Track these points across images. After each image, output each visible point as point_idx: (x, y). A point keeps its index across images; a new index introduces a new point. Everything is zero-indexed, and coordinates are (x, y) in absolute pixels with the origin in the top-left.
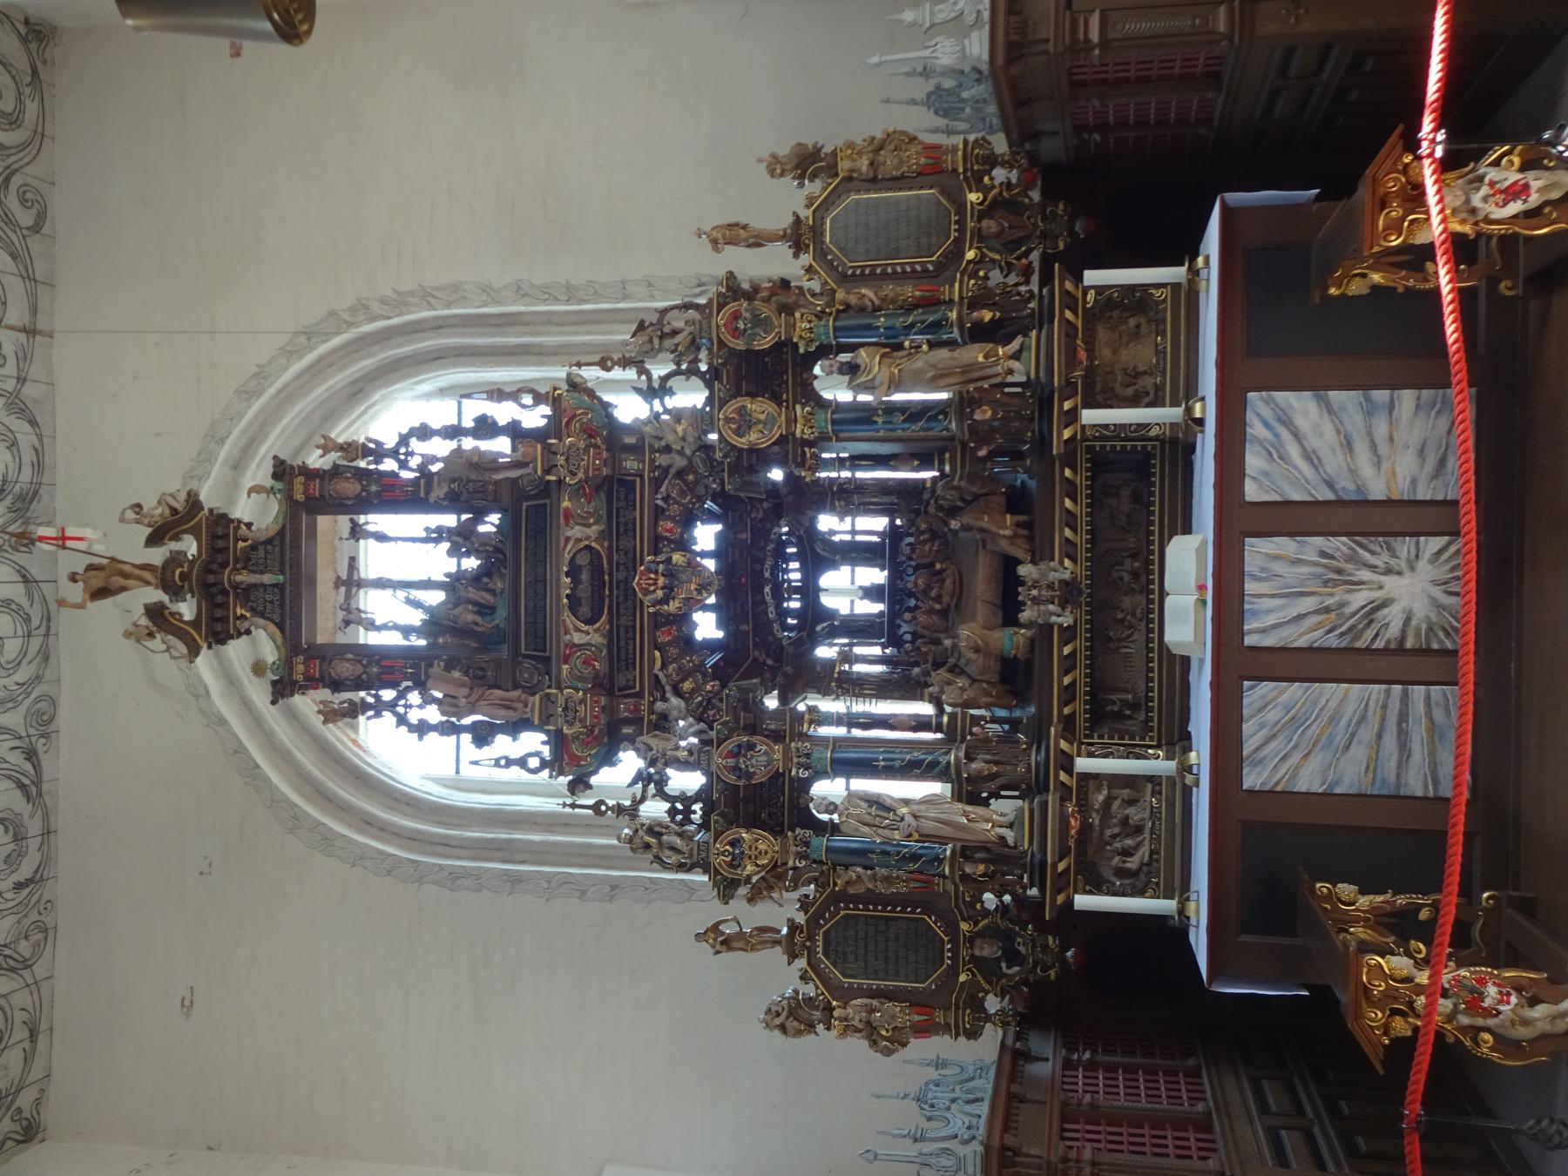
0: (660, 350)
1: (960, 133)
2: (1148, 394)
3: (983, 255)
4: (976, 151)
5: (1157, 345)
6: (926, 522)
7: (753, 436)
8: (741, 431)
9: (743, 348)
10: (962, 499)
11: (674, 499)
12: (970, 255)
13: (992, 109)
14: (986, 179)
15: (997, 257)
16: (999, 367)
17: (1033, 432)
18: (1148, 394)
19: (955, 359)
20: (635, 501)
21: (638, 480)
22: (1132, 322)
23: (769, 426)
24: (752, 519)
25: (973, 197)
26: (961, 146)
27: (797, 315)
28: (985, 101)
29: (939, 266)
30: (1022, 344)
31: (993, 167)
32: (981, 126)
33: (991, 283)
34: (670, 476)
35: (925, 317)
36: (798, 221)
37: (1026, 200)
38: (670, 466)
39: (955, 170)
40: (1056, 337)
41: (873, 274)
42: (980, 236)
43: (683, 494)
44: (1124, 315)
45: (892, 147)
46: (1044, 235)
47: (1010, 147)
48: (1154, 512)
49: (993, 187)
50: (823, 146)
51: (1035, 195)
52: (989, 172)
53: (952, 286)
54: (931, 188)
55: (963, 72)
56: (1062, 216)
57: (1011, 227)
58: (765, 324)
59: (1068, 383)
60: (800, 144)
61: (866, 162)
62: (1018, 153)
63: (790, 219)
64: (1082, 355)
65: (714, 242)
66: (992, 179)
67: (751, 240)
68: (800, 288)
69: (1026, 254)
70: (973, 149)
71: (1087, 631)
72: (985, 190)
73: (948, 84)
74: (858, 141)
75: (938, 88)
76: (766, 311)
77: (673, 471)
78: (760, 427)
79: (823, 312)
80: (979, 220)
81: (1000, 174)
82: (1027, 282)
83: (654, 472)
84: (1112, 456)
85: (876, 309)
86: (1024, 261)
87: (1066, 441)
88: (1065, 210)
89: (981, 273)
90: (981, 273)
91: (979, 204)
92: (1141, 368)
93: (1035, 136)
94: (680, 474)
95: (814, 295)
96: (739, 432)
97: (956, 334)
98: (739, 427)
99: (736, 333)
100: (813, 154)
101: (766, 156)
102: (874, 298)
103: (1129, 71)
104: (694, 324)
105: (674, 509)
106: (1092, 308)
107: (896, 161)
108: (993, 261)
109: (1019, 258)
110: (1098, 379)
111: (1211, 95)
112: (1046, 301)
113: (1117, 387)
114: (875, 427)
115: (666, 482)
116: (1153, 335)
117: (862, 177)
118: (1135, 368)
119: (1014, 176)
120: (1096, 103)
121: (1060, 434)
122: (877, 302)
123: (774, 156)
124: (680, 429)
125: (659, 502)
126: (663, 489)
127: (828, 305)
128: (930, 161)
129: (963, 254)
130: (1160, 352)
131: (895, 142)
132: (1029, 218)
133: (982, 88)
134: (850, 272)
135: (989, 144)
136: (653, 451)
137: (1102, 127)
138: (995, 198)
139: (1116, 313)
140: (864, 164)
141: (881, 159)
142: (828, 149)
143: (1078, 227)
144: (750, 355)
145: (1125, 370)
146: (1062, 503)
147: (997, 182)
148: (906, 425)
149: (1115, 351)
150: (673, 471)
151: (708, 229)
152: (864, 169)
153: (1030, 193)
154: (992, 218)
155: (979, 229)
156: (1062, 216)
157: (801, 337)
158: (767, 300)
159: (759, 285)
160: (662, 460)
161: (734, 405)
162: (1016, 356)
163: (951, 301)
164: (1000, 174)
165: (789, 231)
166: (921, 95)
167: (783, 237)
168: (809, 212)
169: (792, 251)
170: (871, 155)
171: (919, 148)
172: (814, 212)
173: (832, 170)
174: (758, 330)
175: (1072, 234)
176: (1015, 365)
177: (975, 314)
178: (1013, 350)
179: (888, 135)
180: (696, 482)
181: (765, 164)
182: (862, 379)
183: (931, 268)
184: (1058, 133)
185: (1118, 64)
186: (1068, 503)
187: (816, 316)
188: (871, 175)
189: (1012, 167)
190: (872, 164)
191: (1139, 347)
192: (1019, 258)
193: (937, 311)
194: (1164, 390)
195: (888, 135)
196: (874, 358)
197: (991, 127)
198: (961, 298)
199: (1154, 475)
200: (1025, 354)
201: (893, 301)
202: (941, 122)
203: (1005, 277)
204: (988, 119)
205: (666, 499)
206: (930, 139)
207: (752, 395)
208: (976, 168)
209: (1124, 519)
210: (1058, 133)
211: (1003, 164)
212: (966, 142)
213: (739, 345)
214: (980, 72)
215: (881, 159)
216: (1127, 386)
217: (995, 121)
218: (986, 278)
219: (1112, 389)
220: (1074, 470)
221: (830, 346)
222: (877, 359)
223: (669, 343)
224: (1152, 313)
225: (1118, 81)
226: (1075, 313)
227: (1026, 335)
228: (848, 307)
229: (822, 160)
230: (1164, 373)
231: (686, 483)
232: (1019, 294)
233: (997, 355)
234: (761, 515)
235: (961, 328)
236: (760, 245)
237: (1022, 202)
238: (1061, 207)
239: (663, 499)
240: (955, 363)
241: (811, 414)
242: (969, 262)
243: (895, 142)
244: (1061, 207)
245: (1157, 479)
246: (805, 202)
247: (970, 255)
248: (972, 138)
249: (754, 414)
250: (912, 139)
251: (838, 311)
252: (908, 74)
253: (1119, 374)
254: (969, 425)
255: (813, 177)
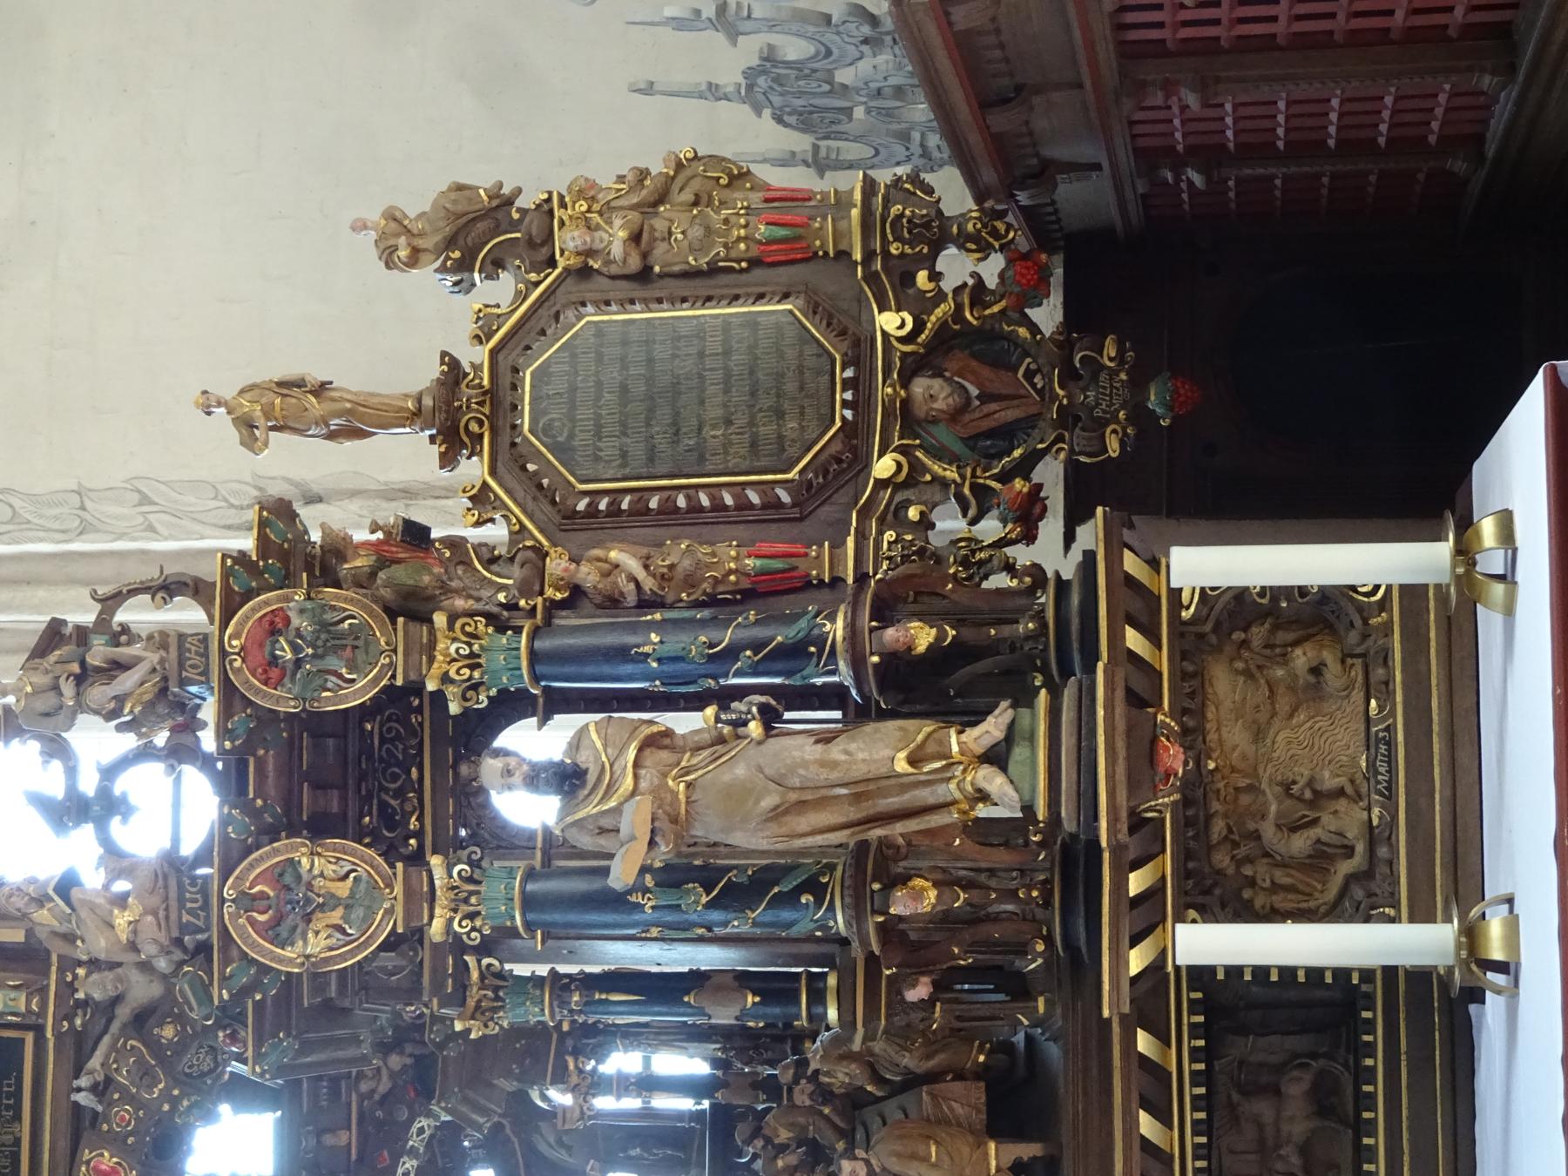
0: (81, 706)
1: (851, 166)
2: (1349, 851)
3: (916, 468)
4: (896, 209)
5: (1368, 720)
6: (791, 1126)
7: (316, 944)
8: (284, 930)
9: (291, 708)
10: (879, 1080)
11: (123, 1090)
12: (884, 467)
13: (920, 111)
14: (922, 277)
15: (951, 474)
16: (952, 786)
17: (1048, 939)
18: (1349, 851)
19: (834, 765)
20: (18, 1094)
21: (29, 1038)
22: (1301, 658)
23: (359, 912)
24: (362, 1097)
25: (890, 322)
26: (858, 196)
27: (440, 619)
28: (899, 91)
29: (807, 493)
30: (1011, 727)
31: (937, 247)
32: (900, 151)
33: (936, 540)
34: (115, 1027)
35: (760, 633)
36: (453, 372)
37: (1023, 332)
38: (117, 1000)
39: (843, 255)
40: (1100, 712)
41: (641, 511)
42: (907, 418)
43: (145, 1075)
44: (1283, 637)
45: (687, 196)
46: (1068, 418)
47: (979, 199)
48: (1372, 1149)
49: (940, 296)
50: (518, 191)
51: (1048, 316)
52: (929, 261)
53: (838, 544)
54: (785, 296)
55: (827, 19)
56: (1113, 373)
57: (985, 398)
58: (354, 645)
59: (1137, 823)
60: (460, 188)
61: (622, 234)
62: (1001, 215)
63: (433, 371)
64: (1174, 757)
65: (246, 425)
66: (935, 276)
67: (335, 422)
68: (455, 544)
69: (1024, 468)
70: (887, 203)
71: (1194, 1007)
72: (920, 306)
73: (794, 49)
74: (606, 180)
75: (770, 58)
76: (348, 605)
77: (123, 1013)
78: (336, 916)
79: (512, 607)
80: (906, 381)
81: (956, 266)
82: (1029, 537)
83: (70, 1018)
84: (1254, 989)
85: (646, 603)
86: (1018, 484)
87: (1134, 980)
88: (1120, 358)
89: (913, 513)
90: (913, 513)
91: (903, 340)
92: (1329, 781)
93: (1044, 173)
94: (143, 1020)
95: (491, 561)
96: (277, 932)
97: (844, 675)
98: (278, 921)
99: (272, 670)
100: (488, 213)
101: (374, 215)
102: (641, 574)
103: (1274, 19)
104: (164, 646)
105: (123, 1116)
106: (1194, 620)
107: (696, 232)
108: (943, 483)
109: (1005, 478)
110: (1216, 806)
111: (1487, 81)
112: (1075, 599)
113: (1268, 830)
114: (637, 917)
115: (106, 1040)
116: (1358, 695)
117: (614, 270)
118: (1310, 783)
119: (992, 269)
120: (1192, 100)
121: (1119, 961)
122: (649, 584)
123: (392, 216)
124: (122, 920)
125: (83, 1098)
126: (95, 1062)
127: (525, 589)
128: (782, 232)
129: (867, 466)
130: (1377, 743)
131: (696, 185)
132: (1029, 375)
133: (884, 59)
134: (581, 506)
135: (929, 191)
136: (68, 964)
137: (1208, 154)
138: (943, 326)
139: (1258, 634)
140: (616, 238)
141: (660, 225)
142: (526, 201)
143: (1152, 401)
144: (314, 724)
145: (1287, 787)
146: (1131, 1124)
147: (948, 285)
148: (716, 916)
149: (1258, 734)
150: (123, 1013)
151: (229, 393)
152: (617, 250)
153: (1034, 314)
154: (938, 374)
155: (906, 403)
156: (1113, 373)
157: (445, 679)
158: (364, 581)
159: (347, 539)
160: (94, 988)
161: (270, 856)
162: (996, 757)
163: (837, 581)
164: (956, 266)
165: (428, 402)
166: (730, 77)
167: (415, 417)
168: (481, 354)
169: (435, 450)
170: (634, 216)
171: (756, 198)
172: (494, 353)
173: (539, 250)
174: (332, 662)
175: (1140, 415)
176: (992, 780)
177: (890, 633)
178: (987, 742)
179: (679, 166)
180: (181, 1047)
181: (373, 235)
182: (590, 810)
183: (785, 497)
184: (1097, 167)
185: (1358, 14)
186: (1147, 1125)
187: (491, 618)
188: (634, 264)
189: (984, 250)
190: (636, 238)
191: (1323, 723)
192: (1005, 478)
193: (795, 618)
194: (1391, 841)
195: (679, 166)
196: (622, 750)
197: (925, 154)
198: (862, 578)
199: (1370, 1050)
200: (1019, 753)
201: (690, 582)
202: (801, 142)
203: (973, 522)
204: (916, 136)
205: (101, 1089)
206: (778, 178)
207: (320, 828)
208: (894, 249)
209: (1295, 1160)
210: (1097, 167)
211: (962, 241)
212: (870, 187)
213: (284, 701)
214: (873, 20)
215: (660, 225)
216: (1294, 829)
217: (934, 140)
218: (926, 524)
219: (1256, 836)
220: (1161, 1036)
221: (523, 694)
222: (631, 754)
223: (99, 693)
224: (1353, 637)
225: (1245, 45)
226: (1151, 634)
227: (1023, 699)
228: (576, 594)
229: (514, 226)
230: (1390, 794)
231: (154, 1046)
232: (1009, 568)
233: (946, 755)
234: (384, 1085)
235: (857, 663)
236: (361, 434)
237: (1012, 339)
238: (1110, 349)
239: (94, 1089)
240: (835, 776)
241: (470, 880)
242: (881, 484)
243: (696, 185)
244: (1110, 349)
245: (1378, 1062)
246: (471, 327)
247: (884, 467)
248: (884, 177)
249: (319, 882)
250: (739, 177)
251: (553, 607)
252: (679, 24)
253: (1271, 793)
254: (880, 926)
255: (495, 265)
